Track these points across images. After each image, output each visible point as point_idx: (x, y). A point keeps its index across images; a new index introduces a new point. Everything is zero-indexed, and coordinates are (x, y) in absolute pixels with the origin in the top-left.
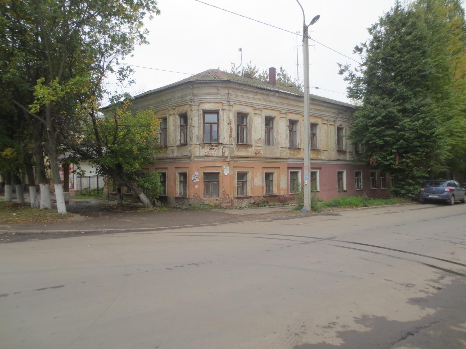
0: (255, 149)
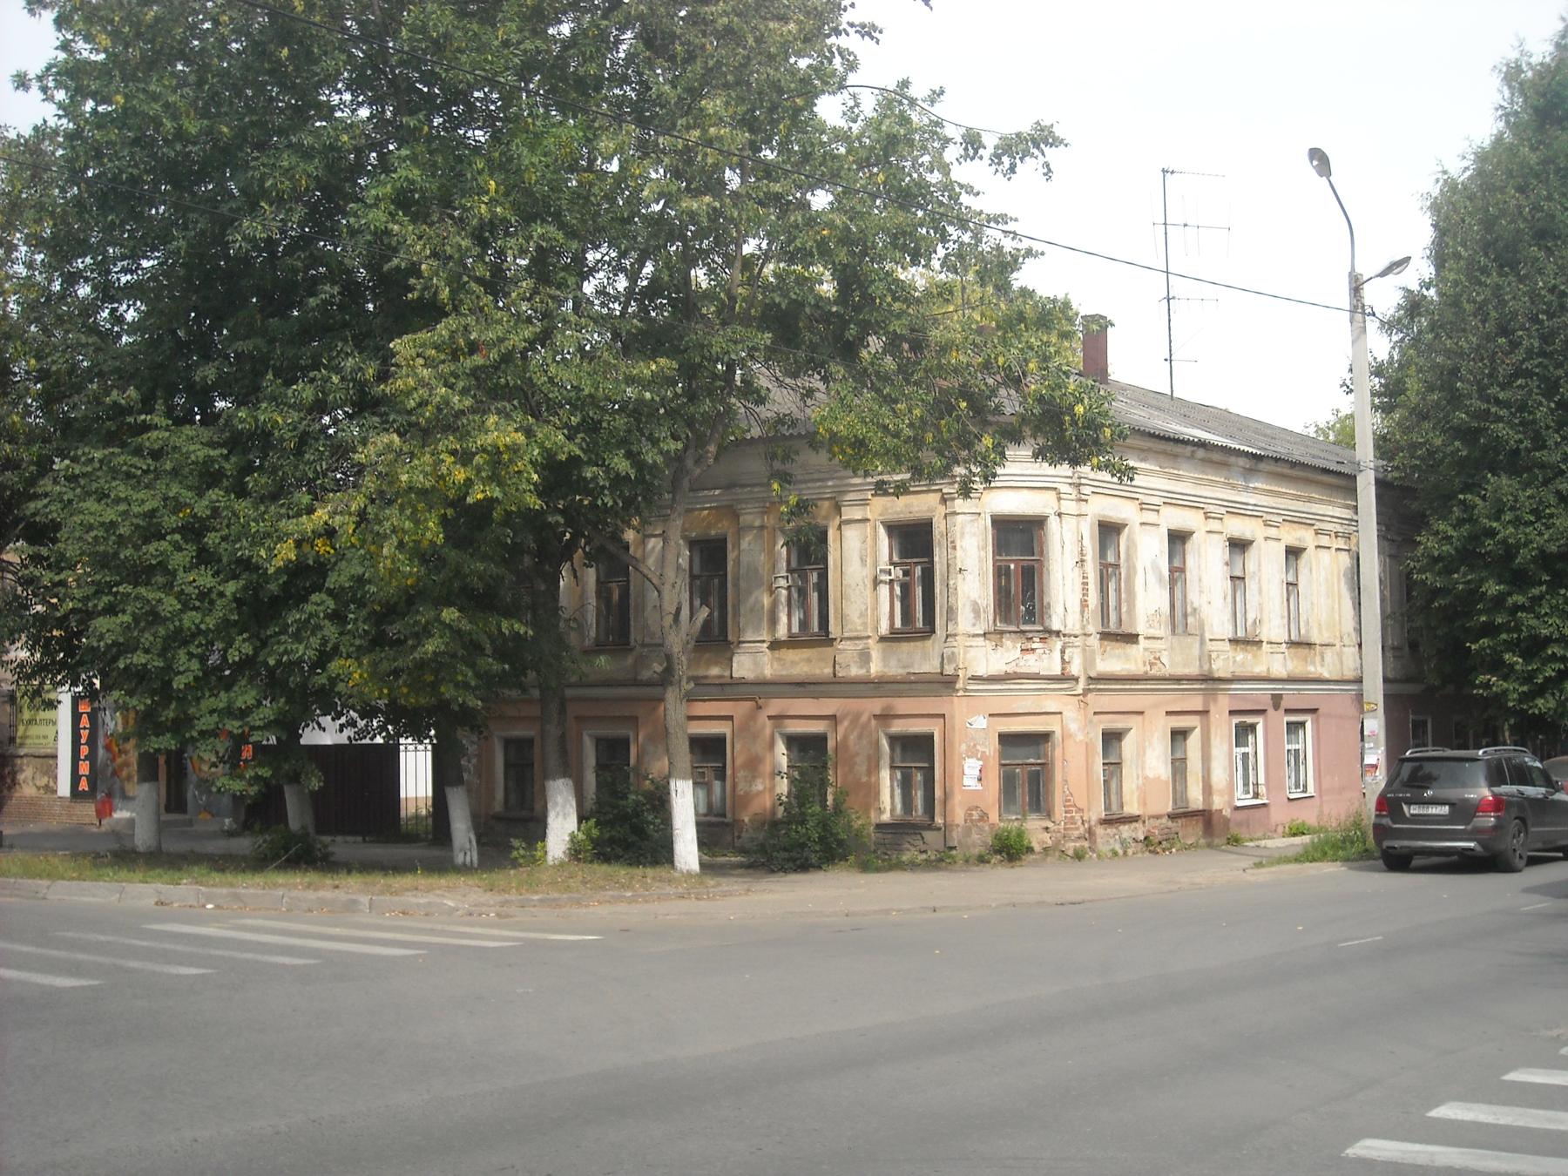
0: (1146, 649)
